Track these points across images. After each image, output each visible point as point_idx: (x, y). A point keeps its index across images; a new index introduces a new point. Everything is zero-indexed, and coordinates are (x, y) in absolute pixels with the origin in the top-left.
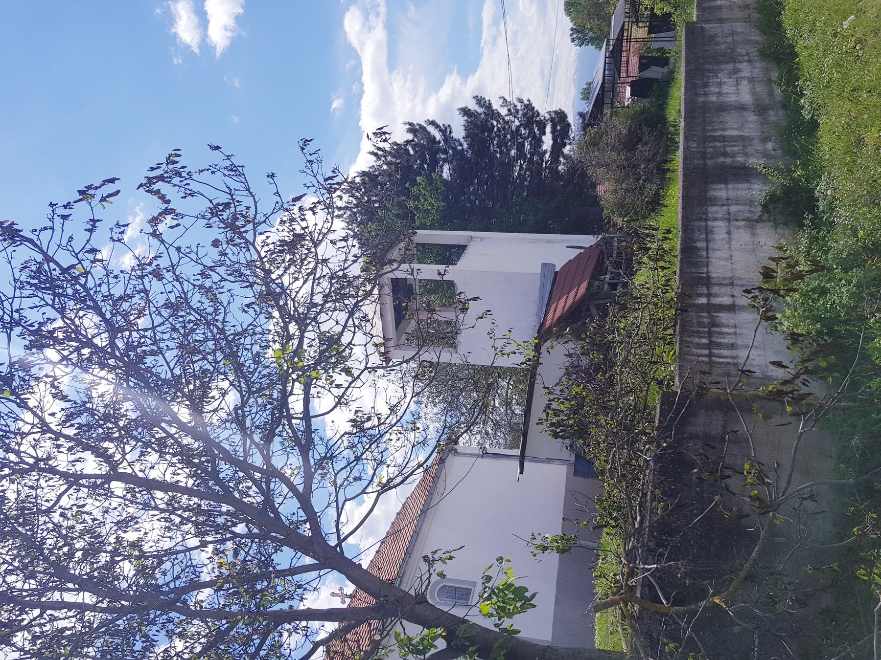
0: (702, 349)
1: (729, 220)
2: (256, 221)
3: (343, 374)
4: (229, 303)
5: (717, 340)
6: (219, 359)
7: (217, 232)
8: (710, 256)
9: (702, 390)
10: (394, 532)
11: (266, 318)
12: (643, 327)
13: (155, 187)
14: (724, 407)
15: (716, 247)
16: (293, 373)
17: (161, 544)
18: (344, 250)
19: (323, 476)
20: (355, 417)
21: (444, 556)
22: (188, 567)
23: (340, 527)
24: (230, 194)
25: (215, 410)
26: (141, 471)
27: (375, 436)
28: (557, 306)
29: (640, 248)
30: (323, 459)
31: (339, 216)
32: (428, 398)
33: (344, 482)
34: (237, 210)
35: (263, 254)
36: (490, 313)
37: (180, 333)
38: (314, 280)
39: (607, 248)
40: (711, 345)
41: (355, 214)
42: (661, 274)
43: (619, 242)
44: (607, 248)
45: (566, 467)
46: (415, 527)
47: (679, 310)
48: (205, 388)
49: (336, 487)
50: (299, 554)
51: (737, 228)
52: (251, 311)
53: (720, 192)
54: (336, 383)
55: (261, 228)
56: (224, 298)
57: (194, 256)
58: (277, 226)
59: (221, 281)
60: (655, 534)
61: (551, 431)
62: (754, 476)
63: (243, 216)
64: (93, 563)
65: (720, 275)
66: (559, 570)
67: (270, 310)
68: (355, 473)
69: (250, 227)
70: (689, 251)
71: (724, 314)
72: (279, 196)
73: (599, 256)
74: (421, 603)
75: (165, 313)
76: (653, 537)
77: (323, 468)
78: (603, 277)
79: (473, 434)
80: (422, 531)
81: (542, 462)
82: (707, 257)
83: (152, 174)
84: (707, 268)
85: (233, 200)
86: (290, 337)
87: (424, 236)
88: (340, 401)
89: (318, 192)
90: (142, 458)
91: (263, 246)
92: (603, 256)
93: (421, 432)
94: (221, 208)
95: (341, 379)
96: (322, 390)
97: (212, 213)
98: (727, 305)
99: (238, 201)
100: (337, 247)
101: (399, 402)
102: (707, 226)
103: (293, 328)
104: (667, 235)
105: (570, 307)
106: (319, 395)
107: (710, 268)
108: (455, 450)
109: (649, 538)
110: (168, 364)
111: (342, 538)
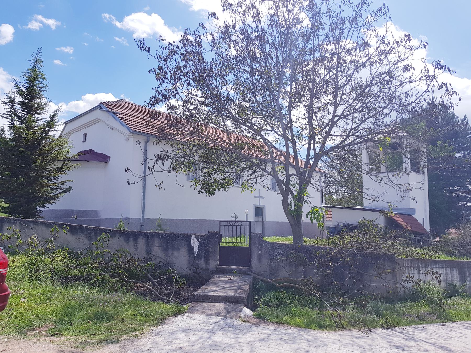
1: (446, 274)
13: (444, 86)
40: (408, 266)
53: (456, 272)
83: (448, 85)
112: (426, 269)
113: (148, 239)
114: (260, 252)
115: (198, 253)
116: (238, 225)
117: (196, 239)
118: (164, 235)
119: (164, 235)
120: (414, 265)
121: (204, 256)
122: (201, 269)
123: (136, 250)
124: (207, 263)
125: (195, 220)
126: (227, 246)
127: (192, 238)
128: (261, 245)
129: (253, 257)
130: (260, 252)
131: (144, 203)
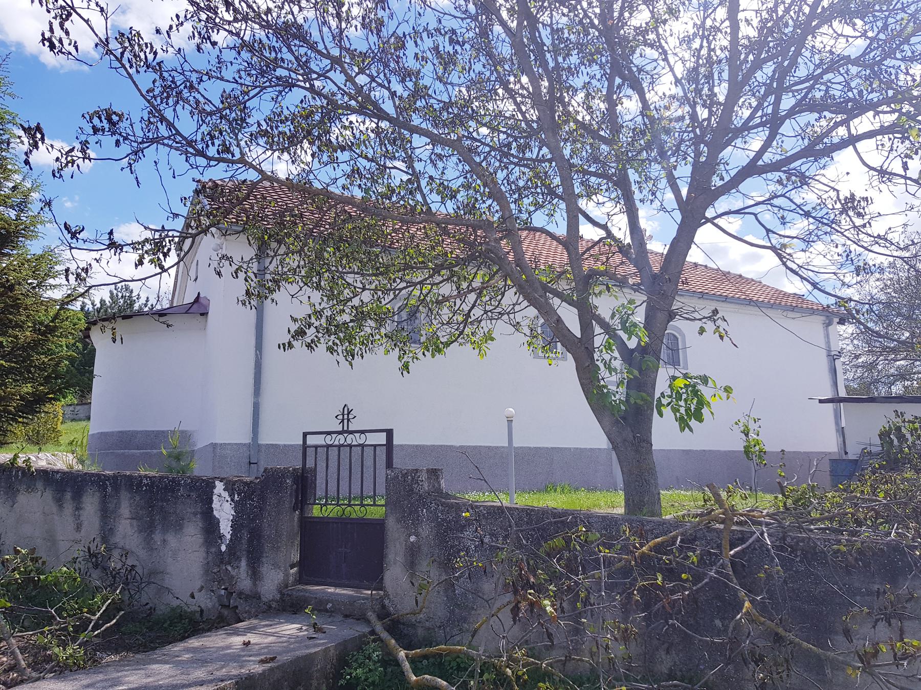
17: (670, 39)
19: (780, 182)
21: (721, 330)
32: (891, 279)
49: (769, 199)
54: (910, 162)
60: (801, 544)
66: (718, 451)
68: (789, 216)
74: (670, 315)
76: (797, 543)
77: (788, 179)
79: (852, 341)
93: (855, 279)
96: (887, 148)
106: (880, 147)
109: (795, 538)
111: (716, 221)
113: (105, 496)
114: (413, 539)
115: (231, 539)
116: (354, 443)
117: (226, 494)
118: (145, 481)
119: (145, 481)
121: (249, 552)
122: (240, 594)
123: (78, 528)
124: (255, 575)
125: (417, 446)
126: (323, 518)
127: (216, 491)
128: (417, 511)
130: (413, 539)
131: (256, 408)
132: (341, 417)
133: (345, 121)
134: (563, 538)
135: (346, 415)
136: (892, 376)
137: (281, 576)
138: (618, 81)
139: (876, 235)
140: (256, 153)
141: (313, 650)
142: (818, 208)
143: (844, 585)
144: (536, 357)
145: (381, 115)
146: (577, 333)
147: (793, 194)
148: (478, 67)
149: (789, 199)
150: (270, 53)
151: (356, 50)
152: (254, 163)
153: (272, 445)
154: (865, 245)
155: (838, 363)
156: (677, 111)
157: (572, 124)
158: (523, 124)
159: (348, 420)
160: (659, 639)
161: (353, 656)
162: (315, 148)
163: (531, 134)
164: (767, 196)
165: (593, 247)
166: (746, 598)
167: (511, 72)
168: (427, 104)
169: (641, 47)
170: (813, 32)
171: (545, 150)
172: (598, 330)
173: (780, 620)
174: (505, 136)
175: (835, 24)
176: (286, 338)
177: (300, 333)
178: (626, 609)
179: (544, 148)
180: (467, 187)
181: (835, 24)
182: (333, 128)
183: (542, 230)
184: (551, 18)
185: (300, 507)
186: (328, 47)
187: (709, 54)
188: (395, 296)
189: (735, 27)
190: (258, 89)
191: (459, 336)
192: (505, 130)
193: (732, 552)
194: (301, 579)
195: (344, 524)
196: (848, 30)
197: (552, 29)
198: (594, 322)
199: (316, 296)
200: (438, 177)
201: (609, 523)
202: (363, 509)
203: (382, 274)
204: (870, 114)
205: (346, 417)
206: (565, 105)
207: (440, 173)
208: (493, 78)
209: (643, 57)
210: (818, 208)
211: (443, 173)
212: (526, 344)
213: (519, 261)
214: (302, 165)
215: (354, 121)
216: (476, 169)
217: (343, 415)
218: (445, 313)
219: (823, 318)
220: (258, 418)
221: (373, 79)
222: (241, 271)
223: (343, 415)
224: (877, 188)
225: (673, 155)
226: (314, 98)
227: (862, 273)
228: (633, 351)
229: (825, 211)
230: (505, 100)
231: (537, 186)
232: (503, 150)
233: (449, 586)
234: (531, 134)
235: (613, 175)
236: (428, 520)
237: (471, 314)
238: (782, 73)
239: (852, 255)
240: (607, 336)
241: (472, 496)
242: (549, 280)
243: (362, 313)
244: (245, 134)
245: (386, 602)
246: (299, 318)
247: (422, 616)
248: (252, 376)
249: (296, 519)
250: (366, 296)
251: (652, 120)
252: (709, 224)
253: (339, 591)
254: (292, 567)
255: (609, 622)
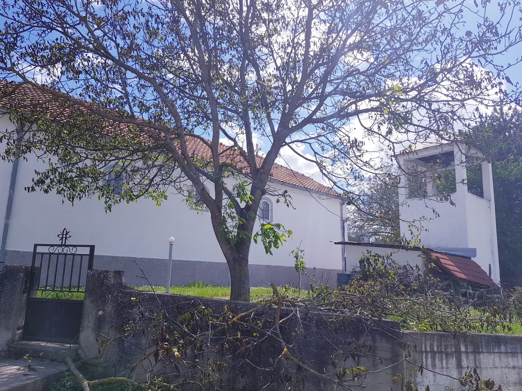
0: (430, 347)
2: (487, 56)
3: (387, 130)
4: (427, 51)
5: (437, 356)
6: (387, 53)
7: (476, 32)
8: (495, 354)
9: (404, 346)
10: (295, 174)
11: (419, 75)
12: (439, 313)
14: (395, 358)
15: (502, 359)
16: (385, 99)
17: (275, 45)
18: (473, 117)
19: (323, 128)
20: (358, 142)
21: (288, 201)
22: (265, 62)
23: (295, 143)
24: (505, 34)
25: (355, 58)
26: (314, 24)
27: (349, 155)
28: (446, 259)
29: (495, 310)
30: (333, 127)
31: (495, 110)
32: (374, 184)
33: (320, 141)
34: (494, 42)
35: (464, 65)
36: (437, 216)
37: (401, 25)
38: (448, 101)
39: (492, 290)
40: (432, 352)
41: (499, 120)
42: (477, 325)
43: (498, 298)
44: (492, 290)
45: (341, 269)
46: (298, 185)
47: (455, 334)
48: (369, 48)
49: (317, 137)
50: (279, 122)
51: (518, 373)
52: (423, 65)
55: (483, 60)
56: (429, 46)
57: (456, 20)
58: (484, 70)
59: (441, 42)
61: (364, 258)
62: (357, 372)
63: (489, 46)
64: (262, 10)
65: (482, 360)
67: (425, 77)
68: (326, 147)
69: (482, 52)
70: (498, 341)
71: (455, 361)
72: (508, 67)
73: (486, 286)
74: (263, 192)
75: (414, 12)
76: (313, 317)
77: (327, 128)
78: (470, 288)
79: (354, 214)
80: (296, 190)
81: (343, 255)
82: (494, 353)
84: (486, 352)
85: (501, 37)
86: (406, 92)
87: (488, 170)
88: (370, 131)
89: (513, 93)
90: (322, 22)
91: (470, 64)
92: (485, 288)
93: (354, 182)
94: (494, 31)
95: (384, 129)
96: (374, 119)
97: (489, 25)
98: (461, 363)
99: (500, 41)
100: (474, 112)
101: (372, 167)
102: (517, 353)
103: (413, 94)
104: (506, 328)
105: (447, 268)
107: (486, 354)
108: (343, 204)
110: (381, 22)
111: (290, 145)
112: (477, 356)
114: (100, 313)
116: (69, 253)
120: (446, 347)
129: (85, 324)
130: (100, 313)
132: (61, 236)
133: (85, 56)
134: (190, 313)
135: (65, 235)
136: (371, 233)
137: (10, 335)
138: (247, 62)
139: (365, 161)
140: (24, 66)
141: (25, 382)
142: (340, 144)
143: (334, 339)
144: (191, 208)
145: (108, 56)
146: (213, 197)
147: (329, 136)
148: (170, 39)
149: (326, 138)
150: (39, 6)
151: (96, 15)
152: (20, 72)
153: (15, 251)
154: (360, 165)
155: (346, 225)
156: (274, 84)
157: (220, 81)
158: (194, 76)
159: (66, 238)
160: (239, 370)
161: (53, 385)
162: (64, 69)
163: (198, 82)
164: (316, 135)
165: (227, 150)
166: (285, 346)
167: (189, 45)
168: (138, 54)
169: (261, 46)
170: (345, 54)
171: (205, 93)
172: (225, 196)
173: (301, 358)
174: (183, 81)
175: (355, 52)
176: (31, 184)
177: (41, 182)
178: (221, 352)
179: (204, 91)
180: (156, 106)
181: (355, 52)
182: (77, 59)
183: (198, 137)
184: (214, 20)
185: (28, 291)
186: (79, 10)
187: (295, 56)
188: (105, 165)
189: (308, 46)
190: (29, 27)
191: (145, 192)
192: (183, 77)
193: (281, 321)
194: (24, 337)
195: (57, 303)
196: (359, 56)
197: (214, 26)
198: (223, 191)
199: (55, 159)
200: (141, 98)
201: (219, 304)
202: (70, 294)
203: (99, 150)
204: (367, 100)
205: (64, 236)
206: (217, 70)
207: (142, 95)
208: (178, 47)
209: (262, 51)
210: (340, 144)
211: (144, 96)
212: (185, 200)
213: (184, 153)
214: (54, 77)
215: (91, 57)
216: (164, 97)
217: (63, 235)
218: (137, 178)
219: (340, 201)
220: (7, 233)
221: (105, 34)
222: (5, 138)
223: (63, 235)
224: (368, 138)
225: (271, 107)
226: (67, 39)
227: (358, 179)
228: (243, 209)
229: (342, 146)
230: (185, 61)
231: (199, 112)
232: (181, 89)
233: (121, 341)
234: (198, 82)
235: (241, 112)
236: (112, 301)
237: (154, 180)
238: (327, 73)
239: (354, 170)
240: (230, 200)
241: (145, 288)
242: (201, 165)
243: (84, 172)
244: (17, 53)
245: (80, 352)
246: (41, 172)
247: (102, 360)
248: (6, 206)
249: (24, 299)
250: (89, 162)
251: (262, 86)
252: (287, 146)
253: (49, 344)
254: (19, 329)
255: (211, 361)
